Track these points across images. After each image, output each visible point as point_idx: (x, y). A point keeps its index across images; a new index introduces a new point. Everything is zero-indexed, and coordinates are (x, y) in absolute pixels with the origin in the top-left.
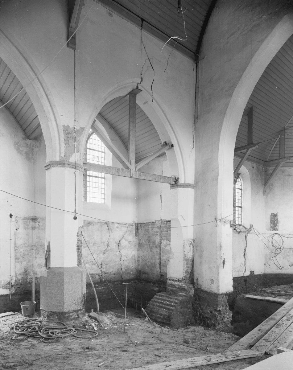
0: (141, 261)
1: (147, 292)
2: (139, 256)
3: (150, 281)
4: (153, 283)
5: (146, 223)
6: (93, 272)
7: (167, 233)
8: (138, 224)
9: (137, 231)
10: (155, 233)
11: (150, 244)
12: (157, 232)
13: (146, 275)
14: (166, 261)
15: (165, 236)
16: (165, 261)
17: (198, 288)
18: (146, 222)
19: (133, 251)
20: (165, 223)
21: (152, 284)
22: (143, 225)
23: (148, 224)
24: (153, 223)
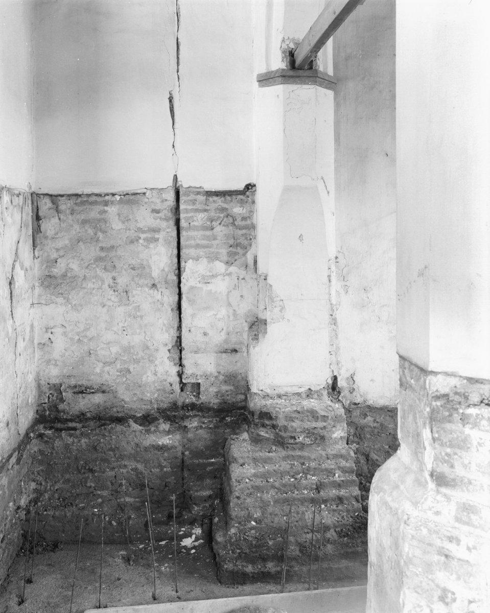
0: (60, 344)
1: (123, 463)
2: (51, 324)
3: (120, 415)
4: (136, 419)
5: (89, 195)
6: (382, 471)
7: (208, 233)
8: (35, 197)
9: (36, 223)
10: (143, 236)
11: (114, 274)
12: (156, 230)
13: (98, 399)
14: (209, 331)
15: (198, 246)
16: (205, 334)
17: (355, 404)
18: (87, 191)
19: (232, 311)
20: (202, 198)
21: (135, 427)
22: (64, 205)
23: (99, 199)
24: (131, 198)
